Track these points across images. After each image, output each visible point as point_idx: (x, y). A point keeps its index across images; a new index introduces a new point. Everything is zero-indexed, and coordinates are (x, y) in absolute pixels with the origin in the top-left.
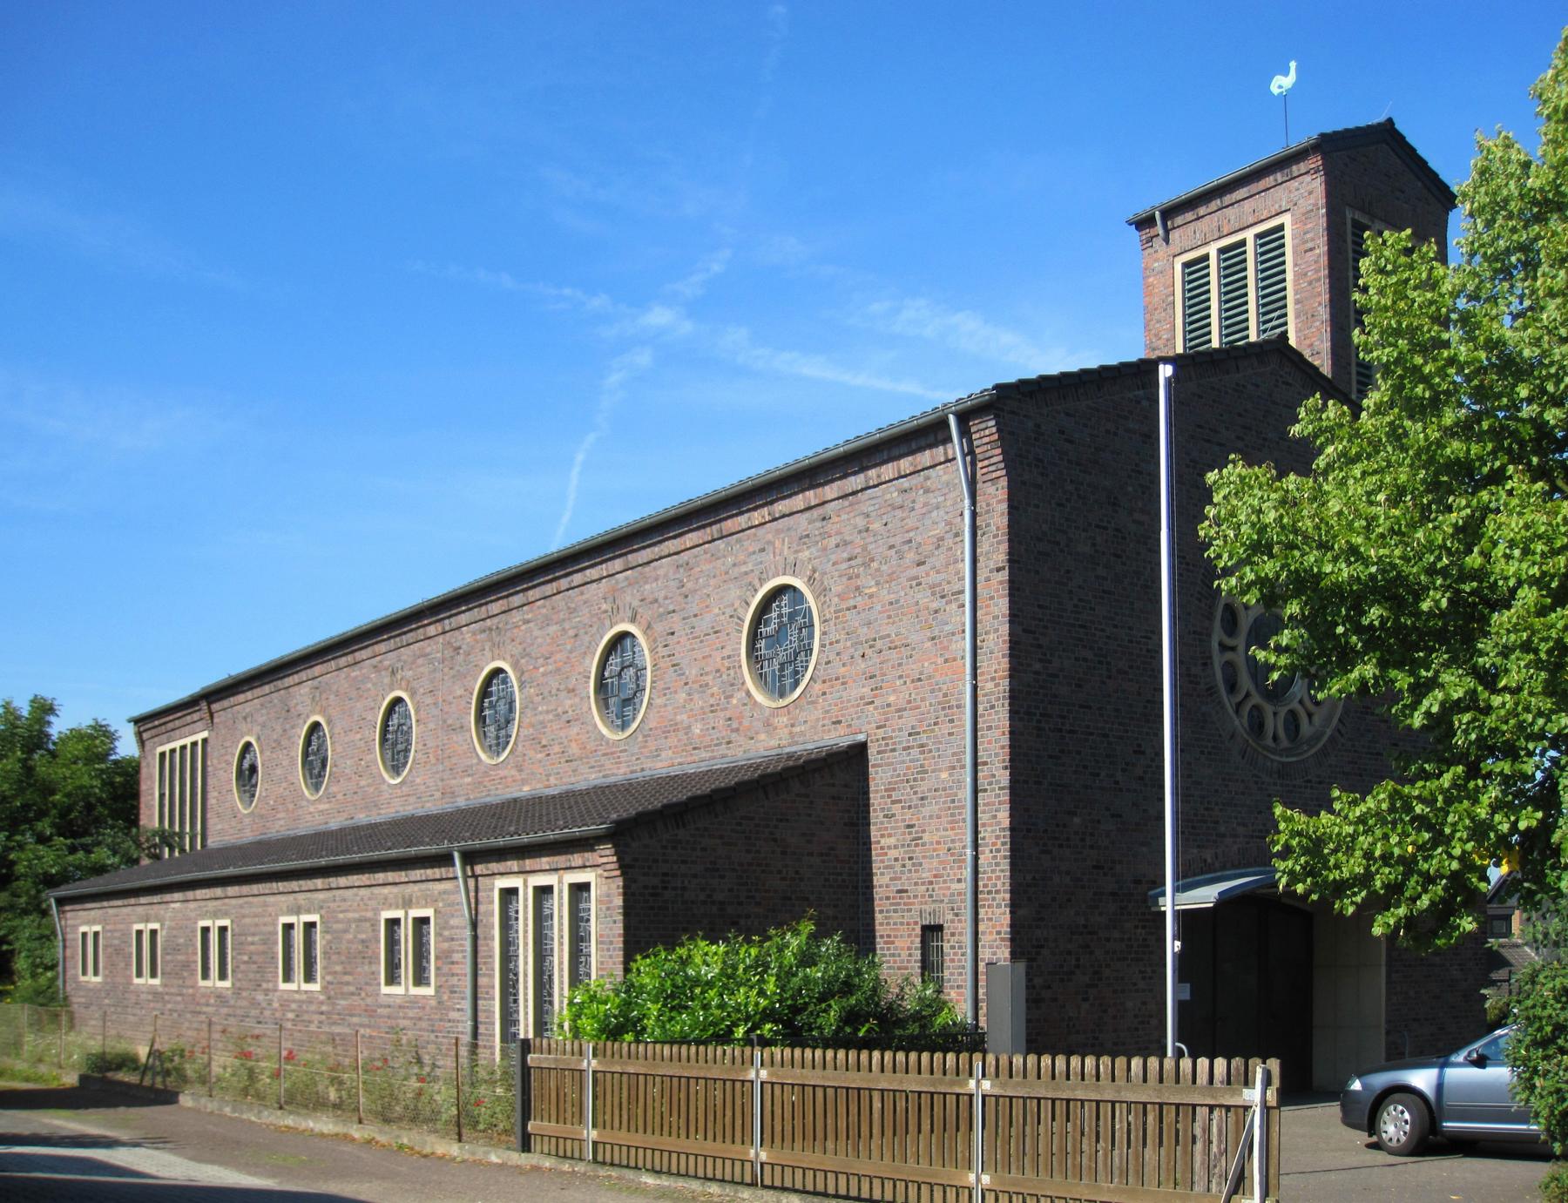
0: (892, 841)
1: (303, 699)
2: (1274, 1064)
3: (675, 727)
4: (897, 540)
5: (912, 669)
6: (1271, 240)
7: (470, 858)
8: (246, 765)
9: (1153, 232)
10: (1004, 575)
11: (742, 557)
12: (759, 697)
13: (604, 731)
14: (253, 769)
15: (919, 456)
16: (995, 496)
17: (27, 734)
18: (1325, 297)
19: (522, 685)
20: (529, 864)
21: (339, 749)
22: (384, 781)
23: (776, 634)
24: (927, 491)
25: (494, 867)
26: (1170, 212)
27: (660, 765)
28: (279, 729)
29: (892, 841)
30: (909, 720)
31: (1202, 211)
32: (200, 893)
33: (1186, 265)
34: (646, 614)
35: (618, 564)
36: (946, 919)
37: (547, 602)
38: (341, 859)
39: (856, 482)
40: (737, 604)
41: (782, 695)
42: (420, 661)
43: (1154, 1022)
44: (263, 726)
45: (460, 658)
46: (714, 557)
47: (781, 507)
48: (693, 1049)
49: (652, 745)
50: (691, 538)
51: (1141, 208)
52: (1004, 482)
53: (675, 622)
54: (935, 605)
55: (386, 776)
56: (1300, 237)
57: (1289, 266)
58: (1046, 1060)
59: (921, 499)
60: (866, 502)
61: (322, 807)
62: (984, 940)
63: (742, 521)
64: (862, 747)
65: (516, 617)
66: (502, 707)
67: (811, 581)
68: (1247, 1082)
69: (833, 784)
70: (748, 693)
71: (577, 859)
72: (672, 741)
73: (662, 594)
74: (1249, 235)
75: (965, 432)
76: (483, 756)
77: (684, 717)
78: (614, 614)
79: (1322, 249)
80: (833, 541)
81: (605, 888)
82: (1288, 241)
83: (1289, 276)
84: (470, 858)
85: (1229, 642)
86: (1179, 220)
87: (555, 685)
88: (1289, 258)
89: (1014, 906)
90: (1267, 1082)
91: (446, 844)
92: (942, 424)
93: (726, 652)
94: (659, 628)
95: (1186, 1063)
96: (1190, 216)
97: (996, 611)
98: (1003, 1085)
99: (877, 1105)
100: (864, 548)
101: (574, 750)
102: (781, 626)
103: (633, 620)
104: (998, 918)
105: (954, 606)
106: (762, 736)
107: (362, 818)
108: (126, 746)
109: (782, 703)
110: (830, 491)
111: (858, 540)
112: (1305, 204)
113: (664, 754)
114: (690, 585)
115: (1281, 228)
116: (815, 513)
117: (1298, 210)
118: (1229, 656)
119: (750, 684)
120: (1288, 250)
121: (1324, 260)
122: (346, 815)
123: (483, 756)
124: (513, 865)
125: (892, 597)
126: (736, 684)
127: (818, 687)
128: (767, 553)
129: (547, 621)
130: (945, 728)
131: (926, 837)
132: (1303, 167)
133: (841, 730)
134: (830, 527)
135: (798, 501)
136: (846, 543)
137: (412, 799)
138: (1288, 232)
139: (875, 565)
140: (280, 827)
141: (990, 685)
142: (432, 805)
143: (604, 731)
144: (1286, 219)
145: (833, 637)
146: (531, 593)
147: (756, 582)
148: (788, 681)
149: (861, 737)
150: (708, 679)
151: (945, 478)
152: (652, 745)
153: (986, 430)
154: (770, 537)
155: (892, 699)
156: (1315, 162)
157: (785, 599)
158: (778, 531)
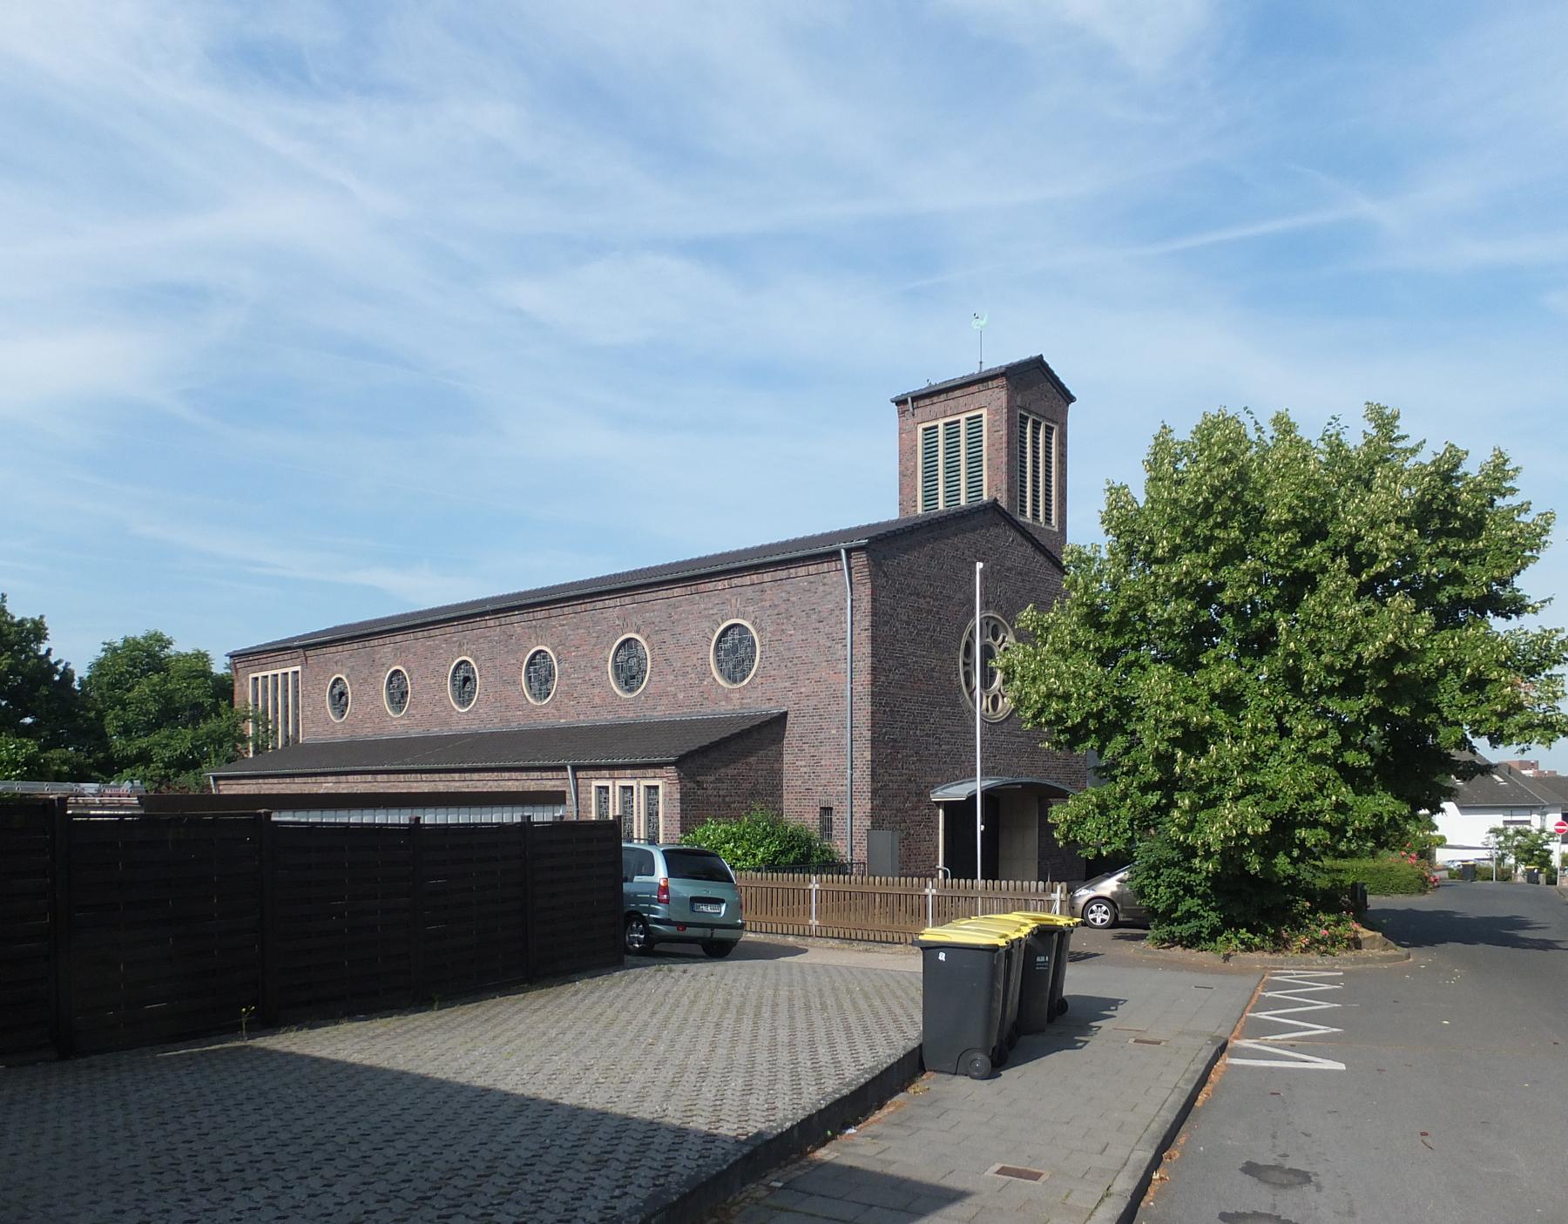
1: (389, 656)
3: (667, 694)
4: (807, 608)
6: (975, 422)
7: (575, 769)
8: (336, 691)
12: (721, 682)
13: (619, 692)
16: (865, 592)
18: (1005, 459)
19: (559, 662)
20: (616, 773)
23: (735, 652)
26: (917, 398)
30: (813, 702)
32: (350, 778)
36: (834, 804)
38: (480, 765)
41: (735, 681)
46: (692, 603)
47: (735, 582)
49: (651, 702)
51: (898, 392)
56: (991, 423)
57: (985, 438)
58: (962, 881)
59: (821, 588)
60: (787, 585)
63: (711, 586)
65: (554, 622)
67: (754, 623)
69: (767, 732)
71: (650, 772)
74: (962, 418)
75: (849, 558)
79: (1004, 432)
80: (767, 604)
83: (985, 444)
86: (921, 403)
94: (655, 638)
95: (949, 881)
96: (927, 401)
101: (597, 701)
102: (734, 645)
103: (638, 632)
107: (435, 730)
108: (219, 667)
109: (735, 686)
110: (767, 577)
112: (995, 405)
116: (757, 588)
117: (990, 409)
119: (715, 674)
120: (985, 428)
121: (1005, 439)
124: (606, 773)
127: (758, 680)
128: (731, 605)
132: (995, 383)
133: (773, 704)
134: (765, 596)
135: (747, 580)
138: (985, 419)
140: (367, 732)
142: (493, 725)
143: (619, 692)
144: (984, 412)
148: (739, 675)
152: (651, 702)
153: (860, 559)
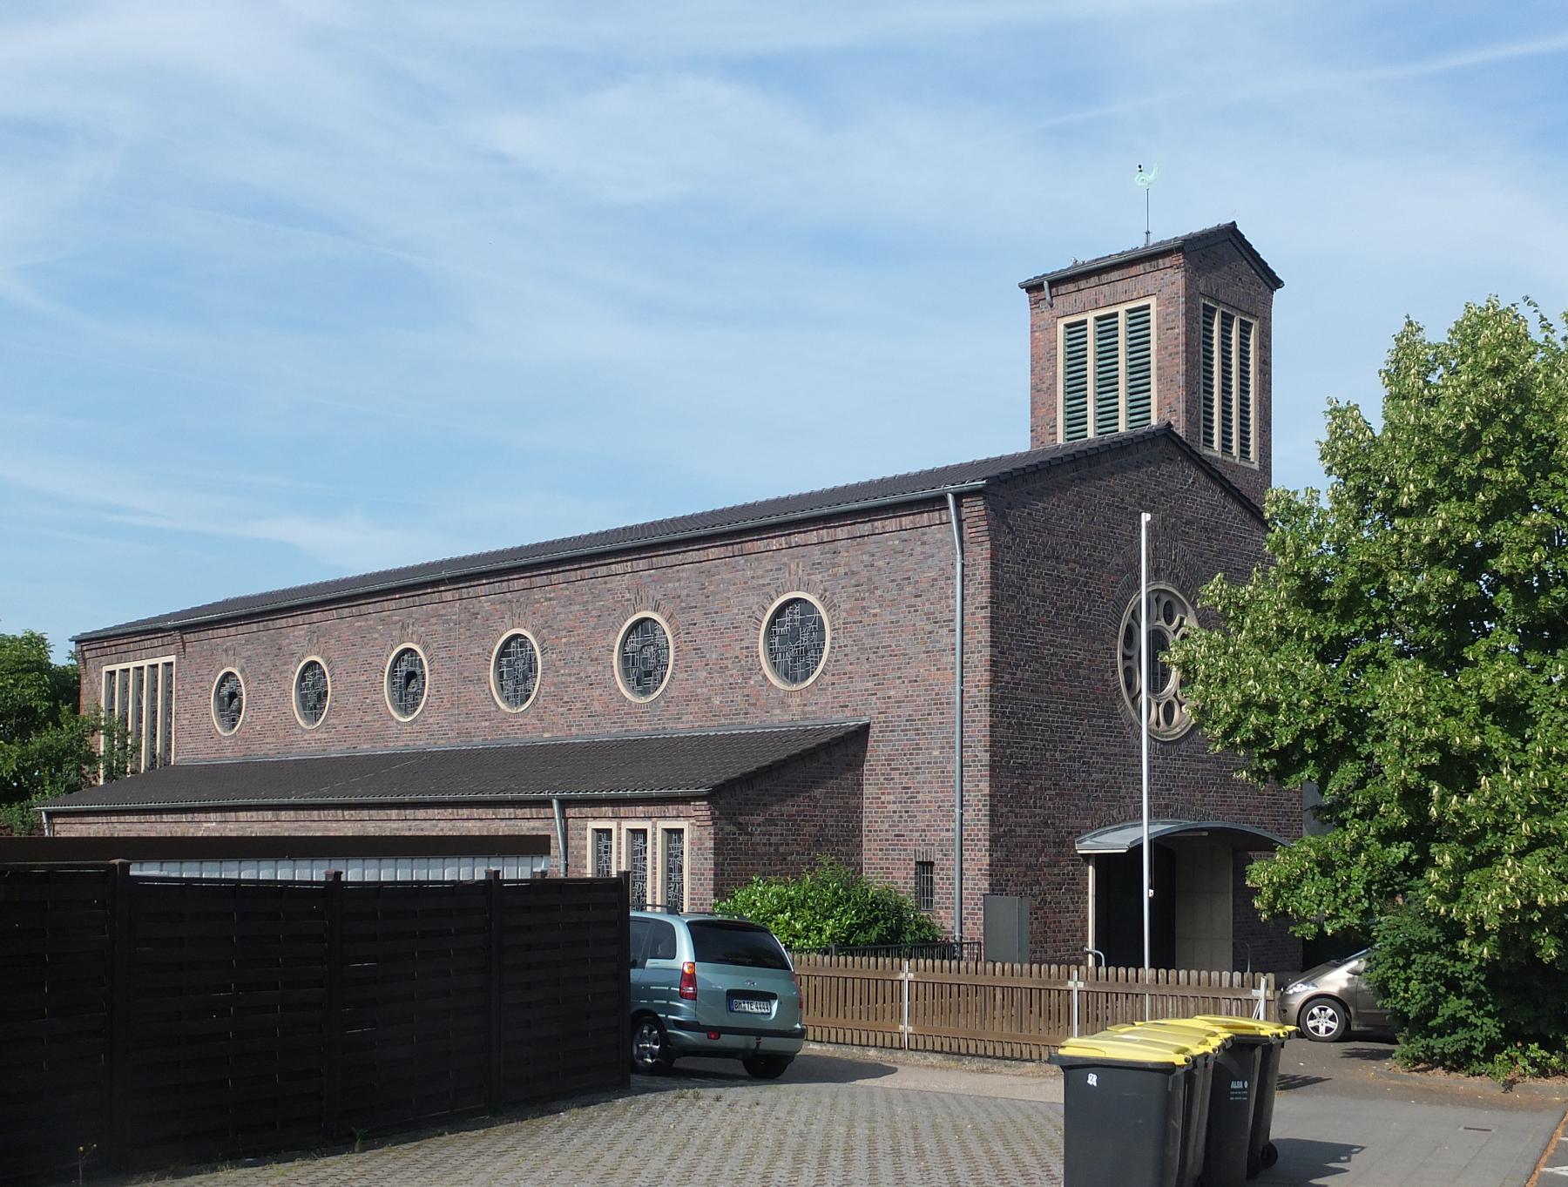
0: (892, 798)
1: (302, 642)
2: (1271, 976)
5: (910, 672)
6: (1139, 316)
7: (565, 804)
8: (225, 691)
9: (1040, 295)
10: (987, 613)
11: (760, 572)
13: (628, 695)
14: (233, 695)
15: (918, 517)
17: (27, 657)
20: (623, 811)
21: (340, 687)
22: (392, 718)
23: (794, 637)
24: (924, 543)
25: (587, 811)
26: (1057, 281)
27: (680, 726)
28: (268, 664)
29: (892, 798)
30: (907, 710)
31: (1082, 284)
33: (1068, 326)
34: (669, 607)
35: (642, 564)
36: (936, 857)
37: (570, 586)
39: (865, 528)
40: (755, 608)
41: (795, 680)
42: (433, 620)
43: (1079, 934)
44: (249, 659)
45: (478, 622)
46: (735, 569)
47: (797, 539)
48: (1026, 966)
49: (673, 709)
50: (713, 553)
52: (987, 545)
53: (697, 615)
54: (929, 628)
55: (395, 714)
56: (1162, 317)
60: (871, 545)
61: (318, 736)
62: (968, 874)
63: (761, 545)
64: (867, 726)
65: (537, 595)
66: (520, 665)
67: (822, 598)
68: (1255, 986)
70: (764, 676)
72: (693, 707)
73: (685, 592)
74: (1121, 310)
75: (958, 506)
76: (502, 706)
77: (705, 690)
78: (636, 605)
79: (1180, 329)
80: (842, 570)
81: (697, 834)
82: (1153, 317)
84: (565, 804)
85: (1129, 653)
86: (1062, 289)
87: (577, 655)
88: (1153, 331)
89: (991, 851)
90: (1267, 986)
91: (545, 794)
92: (940, 501)
93: (744, 644)
94: (682, 618)
96: (1071, 287)
97: (980, 637)
98: (1091, 985)
99: (873, 990)
100: (870, 579)
103: (656, 610)
104: (979, 859)
105: (945, 630)
106: (777, 711)
107: (365, 748)
109: (795, 687)
110: (841, 533)
111: (865, 573)
112: (1167, 292)
113: (684, 718)
114: (712, 588)
115: (1148, 307)
116: (827, 547)
118: (1128, 663)
122: (346, 745)
123: (502, 706)
124: (607, 811)
125: (894, 618)
126: (754, 668)
127: (828, 678)
129: (570, 602)
130: (937, 718)
131: (920, 797)
132: (1168, 261)
134: (839, 559)
135: (813, 537)
136: (853, 573)
137: (422, 736)
138: (1153, 311)
139: (879, 592)
140: (268, 749)
141: (975, 690)
142: (445, 742)
143: (628, 695)
145: (842, 642)
146: (554, 577)
147: (773, 593)
149: (865, 720)
150: (729, 663)
151: (939, 536)
152: (673, 709)
154: (785, 560)
155: (892, 693)
156: (1178, 259)
157: (798, 608)
158: (793, 558)
